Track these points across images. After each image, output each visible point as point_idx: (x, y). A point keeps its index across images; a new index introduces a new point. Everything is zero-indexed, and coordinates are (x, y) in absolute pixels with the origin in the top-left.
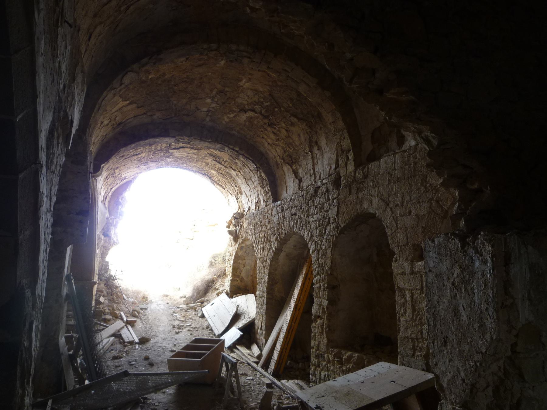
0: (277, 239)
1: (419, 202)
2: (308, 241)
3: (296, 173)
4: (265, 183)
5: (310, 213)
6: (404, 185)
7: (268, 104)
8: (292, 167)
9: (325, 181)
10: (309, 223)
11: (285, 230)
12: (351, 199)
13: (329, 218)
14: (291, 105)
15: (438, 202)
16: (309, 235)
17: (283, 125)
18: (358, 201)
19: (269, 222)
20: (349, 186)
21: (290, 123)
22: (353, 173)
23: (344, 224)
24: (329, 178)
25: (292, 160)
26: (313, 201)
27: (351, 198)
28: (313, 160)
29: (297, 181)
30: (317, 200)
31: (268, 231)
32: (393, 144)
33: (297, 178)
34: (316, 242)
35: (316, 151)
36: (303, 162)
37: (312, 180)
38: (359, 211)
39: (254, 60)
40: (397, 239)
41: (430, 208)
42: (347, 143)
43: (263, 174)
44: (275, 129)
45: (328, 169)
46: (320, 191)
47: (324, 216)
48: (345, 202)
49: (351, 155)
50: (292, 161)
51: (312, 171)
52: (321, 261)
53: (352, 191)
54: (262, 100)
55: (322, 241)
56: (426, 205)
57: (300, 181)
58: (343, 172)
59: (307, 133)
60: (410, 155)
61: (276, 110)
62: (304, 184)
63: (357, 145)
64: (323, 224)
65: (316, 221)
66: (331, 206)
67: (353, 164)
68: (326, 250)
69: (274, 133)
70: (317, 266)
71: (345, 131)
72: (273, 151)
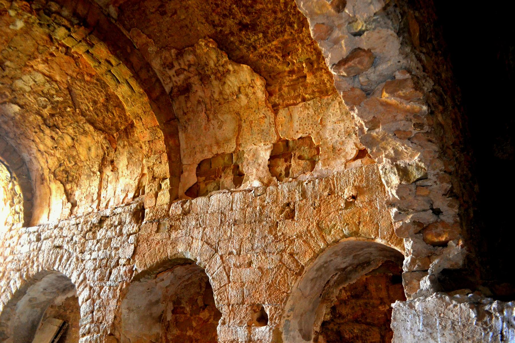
0: (21, 276)
1: (264, 253)
2: (77, 285)
3: (69, 195)
4: (16, 200)
5: (87, 249)
6: (244, 230)
7: (61, 99)
8: (64, 186)
9: (119, 210)
10: (82, 261)
11: (38, 266)
12: (159, 237)
13: (119, 258)
14: (91, 108)
15: (291, 255)
16: (81, 277)
17: (71, 131)
18: (169, 242)
19: (12, 252)
20: (157, 222)
21: (82, 130)
22: (166, 207)
23: (142, 269)
24: (127, 208)
25: (67, 177)
26: (94, 233)
27: (158, 237)
28: (101, 182)
29: (69, 205)
30: (100, 234)
31: (7, 264)
32: (228, 180)
33: (69, 201)
34: (91, 288)
35: (108, 171)
36: (84, 181)
37: (95, 205)
38: (169, 254)
39: (73, 35)
40: (226, 295)
41: (280, 261)
42: (163, 169)
43: (18, 189)
44: (57, 133)
45: (122, 197)
46: (108, 222)
47: (110, 255)
48: (148, 241)
49: (166, 184)
50: (67, 178)
51: (95, 196)
52: (97, 315)
53: (162, 227)
54: (53, 92)
55: (101, 288)
56: (275, 257)
57: (74, 205)
58: (149, 203)
59: (102, 148)
60: (256, 196)
61: (69, 109)
62: (80, 211)
63: (176, 173)
64: (106, 267)
65: (95, 259)
66: (124, 242)
67: (168, 196)
68: (108, 300)
69: (52, 138)
70: (89, 320)
71: (165, 155)
72: (42, 161)
